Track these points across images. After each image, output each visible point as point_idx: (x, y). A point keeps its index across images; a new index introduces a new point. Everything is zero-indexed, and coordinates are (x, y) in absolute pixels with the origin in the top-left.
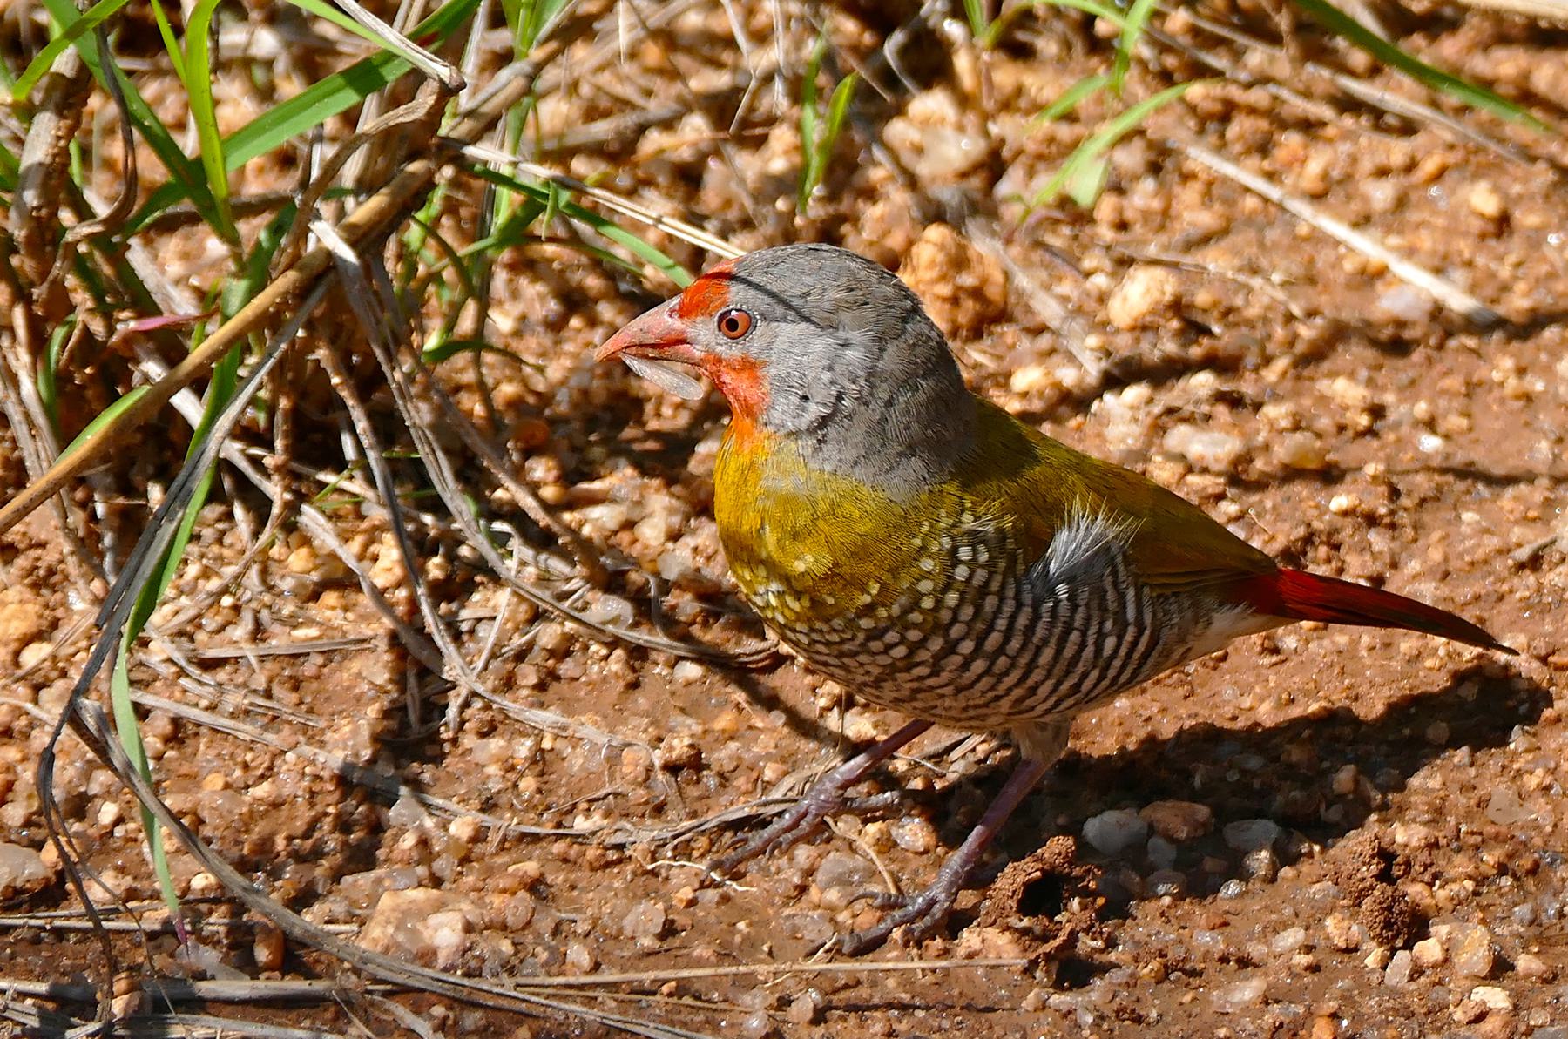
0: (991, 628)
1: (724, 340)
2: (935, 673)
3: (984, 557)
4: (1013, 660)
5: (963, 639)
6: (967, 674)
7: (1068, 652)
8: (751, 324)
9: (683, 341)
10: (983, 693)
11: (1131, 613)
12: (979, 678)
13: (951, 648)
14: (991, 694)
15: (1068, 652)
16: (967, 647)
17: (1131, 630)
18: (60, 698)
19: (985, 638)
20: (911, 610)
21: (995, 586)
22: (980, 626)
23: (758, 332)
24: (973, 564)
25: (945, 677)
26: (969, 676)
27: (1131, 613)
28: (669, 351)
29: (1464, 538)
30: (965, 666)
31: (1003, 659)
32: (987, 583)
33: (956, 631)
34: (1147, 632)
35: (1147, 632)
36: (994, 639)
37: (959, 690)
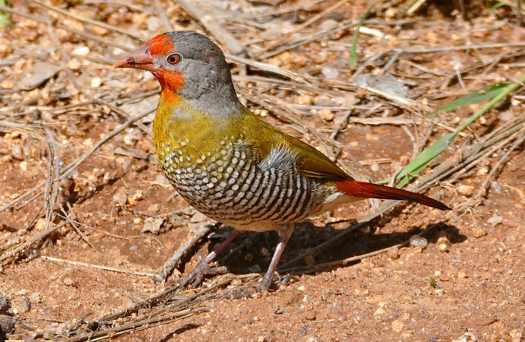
0: (244, 182)
1: (168, 64)
2: (224, 196)
3: (244, 157)
4: (254, 193)
5: (234, 184)
6: (237, 197)
7: (275, 193)
8: (180, 59)
9: (151, 63)
10: (243, 206)
11: (299, 185)
12: (242, 199)
13: (230, 187)
14: (246, 207)
15: (275, 193)
16: (236, 188)
17: (299, 191)
18: (321, 29)
19: (242, 186)
20: (214, 170)
21: (247, 168)
22: (241, 180)
23: (182, 62)
24: (239, 159)
25: (228, 199)
26: (237, 199)
27: (299, 185)
28: (143, 66)
29: (486, 223)
30: (235, 194)
31: (250, 193)
32: (244, 166)
33: (232, 181)
34: (305, 192)
35: (305, 192)
36: (246, 187)
37: (235, 204)
